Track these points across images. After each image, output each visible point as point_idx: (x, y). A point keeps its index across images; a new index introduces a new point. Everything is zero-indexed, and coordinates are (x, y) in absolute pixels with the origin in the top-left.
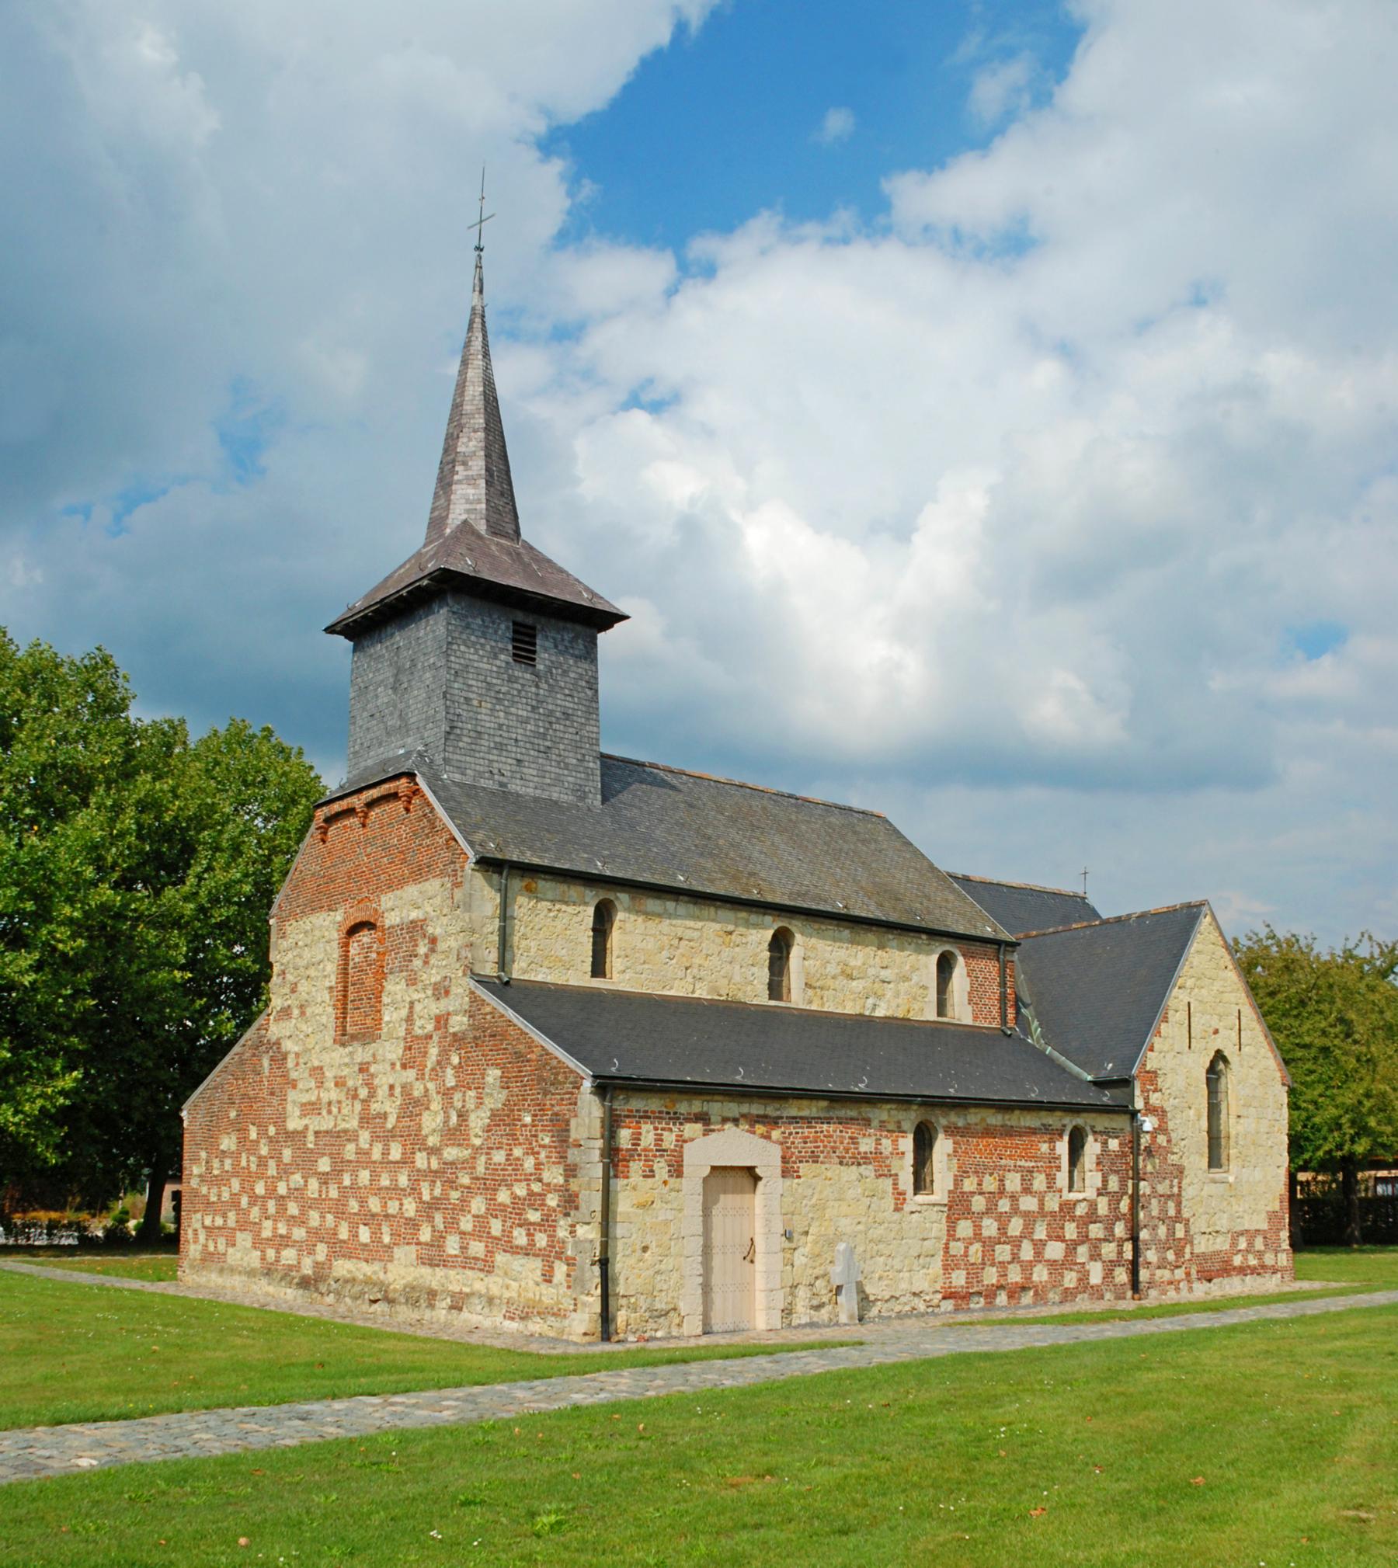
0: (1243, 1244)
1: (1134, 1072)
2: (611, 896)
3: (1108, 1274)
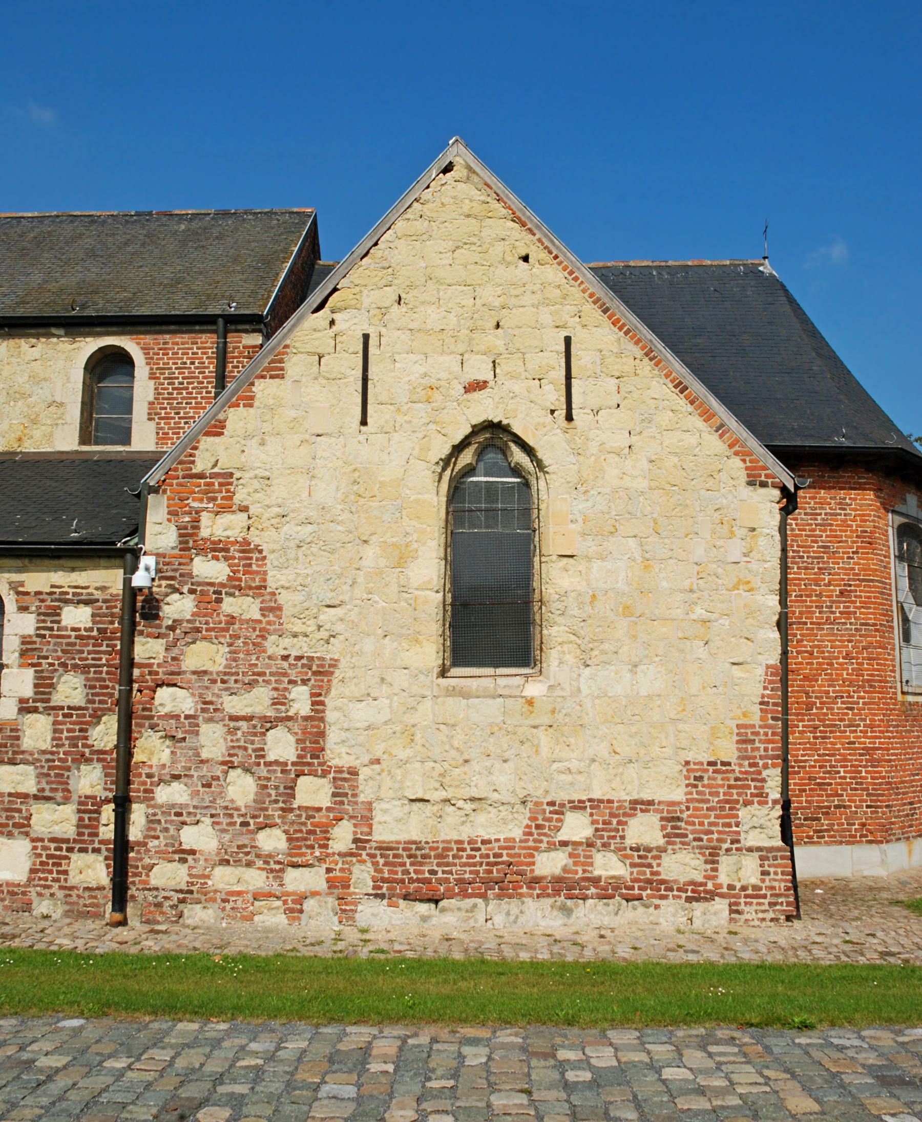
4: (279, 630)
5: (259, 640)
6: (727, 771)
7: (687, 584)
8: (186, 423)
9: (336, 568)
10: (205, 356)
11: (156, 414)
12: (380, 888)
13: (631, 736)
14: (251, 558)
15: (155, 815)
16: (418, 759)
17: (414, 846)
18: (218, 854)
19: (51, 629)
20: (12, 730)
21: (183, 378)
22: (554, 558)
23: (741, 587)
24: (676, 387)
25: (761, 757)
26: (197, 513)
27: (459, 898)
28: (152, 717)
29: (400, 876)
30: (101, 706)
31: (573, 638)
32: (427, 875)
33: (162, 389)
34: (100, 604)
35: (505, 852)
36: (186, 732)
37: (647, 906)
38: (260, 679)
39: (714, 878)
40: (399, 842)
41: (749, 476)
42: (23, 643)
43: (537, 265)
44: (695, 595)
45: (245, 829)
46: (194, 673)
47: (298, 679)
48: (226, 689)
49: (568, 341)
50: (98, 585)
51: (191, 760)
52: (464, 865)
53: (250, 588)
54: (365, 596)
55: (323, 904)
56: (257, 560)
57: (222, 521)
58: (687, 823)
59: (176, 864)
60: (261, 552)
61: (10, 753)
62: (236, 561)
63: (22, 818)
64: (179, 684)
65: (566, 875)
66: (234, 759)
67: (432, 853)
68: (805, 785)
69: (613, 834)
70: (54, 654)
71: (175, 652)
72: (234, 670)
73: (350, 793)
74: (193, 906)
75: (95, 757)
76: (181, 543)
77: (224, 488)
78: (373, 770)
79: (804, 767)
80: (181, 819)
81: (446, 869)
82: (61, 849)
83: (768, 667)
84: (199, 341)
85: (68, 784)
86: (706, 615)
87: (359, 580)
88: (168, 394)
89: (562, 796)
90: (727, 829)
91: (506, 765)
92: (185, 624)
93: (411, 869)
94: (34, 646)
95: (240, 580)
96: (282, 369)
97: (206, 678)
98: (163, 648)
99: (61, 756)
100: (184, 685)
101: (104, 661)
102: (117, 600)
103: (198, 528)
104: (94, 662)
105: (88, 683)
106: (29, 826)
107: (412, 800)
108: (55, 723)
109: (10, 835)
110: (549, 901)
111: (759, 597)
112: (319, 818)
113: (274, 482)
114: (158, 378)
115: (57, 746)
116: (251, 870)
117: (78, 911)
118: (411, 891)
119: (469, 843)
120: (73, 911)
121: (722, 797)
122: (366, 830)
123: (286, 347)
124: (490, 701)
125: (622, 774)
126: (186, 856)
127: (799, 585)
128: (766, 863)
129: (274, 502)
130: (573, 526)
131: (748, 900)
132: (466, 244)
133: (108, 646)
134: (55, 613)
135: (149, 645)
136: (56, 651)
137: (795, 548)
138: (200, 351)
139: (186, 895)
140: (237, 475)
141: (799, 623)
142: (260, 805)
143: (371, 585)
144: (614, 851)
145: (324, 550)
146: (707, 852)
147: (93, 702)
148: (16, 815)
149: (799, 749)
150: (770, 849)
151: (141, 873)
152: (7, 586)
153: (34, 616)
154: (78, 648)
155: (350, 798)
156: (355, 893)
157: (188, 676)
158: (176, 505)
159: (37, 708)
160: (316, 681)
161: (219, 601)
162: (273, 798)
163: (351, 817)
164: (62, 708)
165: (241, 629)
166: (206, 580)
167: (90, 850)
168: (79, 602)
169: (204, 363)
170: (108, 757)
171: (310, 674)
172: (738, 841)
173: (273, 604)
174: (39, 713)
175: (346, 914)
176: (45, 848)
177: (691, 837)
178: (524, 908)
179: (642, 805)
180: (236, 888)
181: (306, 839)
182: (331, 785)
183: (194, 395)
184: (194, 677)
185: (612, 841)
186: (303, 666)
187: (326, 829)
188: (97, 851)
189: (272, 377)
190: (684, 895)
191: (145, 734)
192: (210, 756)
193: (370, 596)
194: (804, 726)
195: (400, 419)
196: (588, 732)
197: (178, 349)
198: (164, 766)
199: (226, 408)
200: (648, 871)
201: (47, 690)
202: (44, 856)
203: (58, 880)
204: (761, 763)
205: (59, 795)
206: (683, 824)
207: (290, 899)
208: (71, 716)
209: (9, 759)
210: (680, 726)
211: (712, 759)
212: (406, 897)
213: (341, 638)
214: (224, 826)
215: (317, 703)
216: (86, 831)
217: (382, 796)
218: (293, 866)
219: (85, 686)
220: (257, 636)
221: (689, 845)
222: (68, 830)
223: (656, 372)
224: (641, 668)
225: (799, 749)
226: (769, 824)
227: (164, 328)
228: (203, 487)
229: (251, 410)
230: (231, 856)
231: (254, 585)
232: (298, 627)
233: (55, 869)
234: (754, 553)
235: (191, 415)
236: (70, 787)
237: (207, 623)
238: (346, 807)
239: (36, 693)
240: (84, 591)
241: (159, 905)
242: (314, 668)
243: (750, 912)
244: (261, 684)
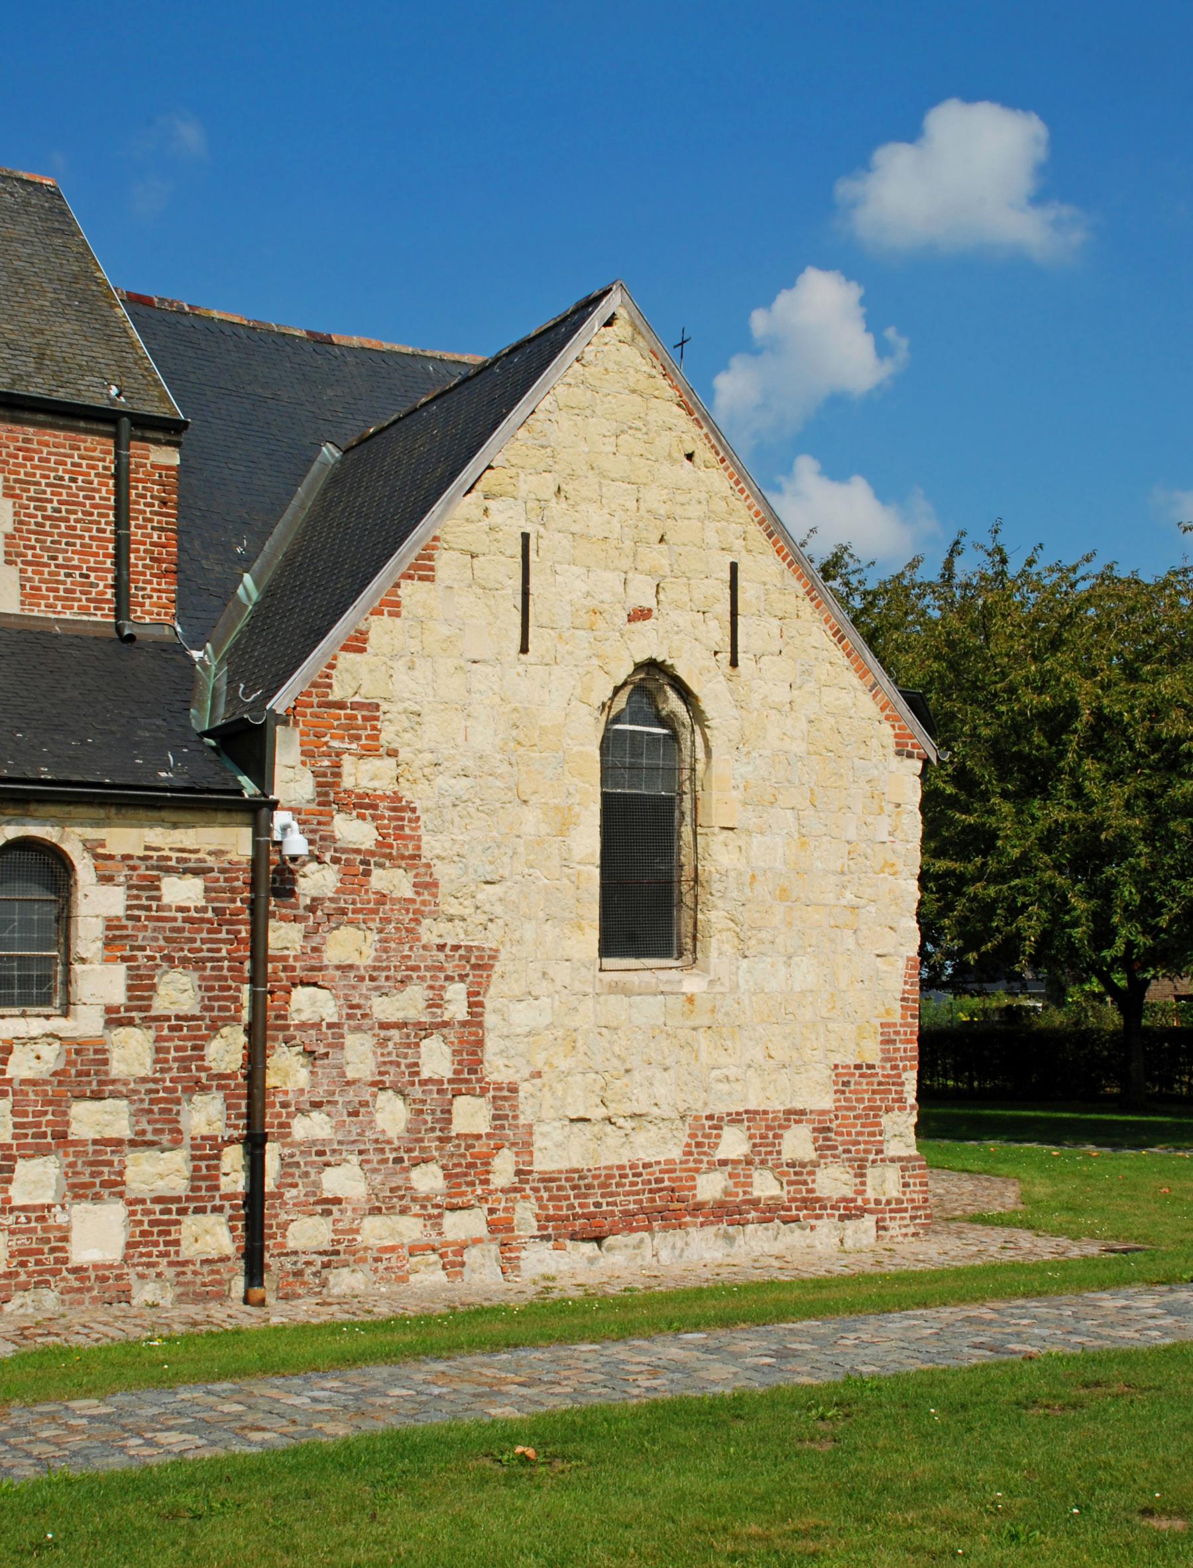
0: (733, 1144)
1: (280, 702)
4: (435, 912)
5: (413, 925)
6: (872, 1075)
7: (838, 866)
8: (68, 575)
9: (495, 834)
10: (93, 472)
11: (19, 555)
12: (546, 1228)
13: (785, 1038)
14: (402, 819)
15: (292, 1156)
16: (580, 1070)
17: (576, 1176)
18: (369, 1200)
19: (149, 908)
20: (96, 1052)
21: (60, 502)
22: (716, 830)
23: (887, 870)
24: (834, 635)
25: (902, 1059)
26: (338, 755)
27: (625, 1233)
28: (287, 1027)
29: (564, 1212)
30: (222, 1014)
31: (732, 925)
32: (592, 1209)
33: (26, 515)
34: (215, 874)
35: (666, 1176)
36: (329, 1045)
37: (803, 1228)
38: (415, 975)
39: (862, 1192)
40: (560, 1172)
41: (898, 744)
42: (108, 928)
43: (703, 468)
44: (845, 878)
45: (399, 1166)
46: (338, 968)
47: (455, 975)
48: (377, 988)
49: (734, 567)
50: (212, 848)
51: (334, 1082)
53: (403, 857)
54: (526, 871)
55: (486, 1253)
56: (410, 821)
57: (368, 767)
58: (837, 1133)
59: (317, 1217)
60: (414, 810)
61: (95, 1083)
62: (386, 822)
63: (115, 1173)
64: (320, 983)
65: (728, 1199)
66: (386, 1078)
67: (596, 1183)
69: (769, 1149)
70: (155, 944)
71: (316, 941)
72: (384, 964)
73: (511, 1114)
74: (341, 1270)
75: (214, 1083)
76: (319, 794)
77: (368, 724)
78: (533, 1085)
80: (323, 1158)
81: (610, 1200)
82: (169, 1211)
83: (909, 959)
84: (82, 445)
85: (178, 1122)
86: (856, 901)
87: (518, 850)
88: (37, 524)
89: (720, 1109)
90: (872, 1139)
91: (666, 1075)
92: (327, 904)
94: (125, 933)
95: (391, 846)
96: (432, 569)
97: (352, 975)
98: (301, 936)
99: (168, 1084)
100: (326, 984)
101: (224, 953)
102: (238, 870)
103: (339, 775)
104: (210, 955)
105: (204, 984)
106: (123, 1183)
107: (572, 1120)
108: (158, 1039)
109: (97, 1198)
110: (712, 1230)
111: (902, 882)
112: (480, 1147)
113: (425, 719)
114: (19, 497)
115: (162, 1070)
116: (405, 1218)
117: (195, 1293)
118: (577, 1229)
119: (631, 1168)
120: (187, 1294)
121: (867, 1104)
122: (527, 1158)
123: (436, 539)
124: (651, 999)
125: (775, 1081)
126: (330, 1207)
129: (426, 747)
130: (734, 793)
132: (631, 428)
133: (228, 932)
134: (153, 886)
135: (282, 931)
136: (156, 939)
138: (84, 462)
139: (331, 1257)
140: (384, 707)
142: (414, 1132)
143: (532, 857)
144: (771, 1169)
145: (482, 811)
146: (856, 1164)
147: (211, 1009)
148: (106, 1169)
150: (909, 1159)
151: (276, 1233)
152: (80, 845)
153: (122, 889)
154: (186, 934)
155: (511, 1121)
156: (519, 1237)
157: (331, 972)
158: (311, 743)
159: (132, 1018)
160: (474, 976)
161: (367, 873)
162: (430, 1125)
163: (513, 1144)
164: (168, 1018)
165: (392, 910)
166: (351, 846)
167: (209, 1209)
168: (186, 871)
169: (91, 483)
170: (232, 1083)
171: (468, 967)
172: (879, 1152)
173: (428, 879)
174: (134, 1026)
175: (509, 1264)
176: (147, 1212)
177: (841, 1148)
178: (689, 1239)
179: (795, 1115)
180: (388, 1243)
181: (466, 1174)
182: (490, 1106)
183: (78, 532)
184: (338, 973)
185: (769, 1157)
186: (461, 957)
187: (486, 1160)
188: (218, 1209)
189: (421, 578)
190: (837, 1213)
191: (279, 1050)
192: (357, 1076)
193: (531, 871)
196: (746, 1034)
197: (49, 453)
198: (302, 1091)
199: (367, 615)
200: (804, 1188)
201: (146, 994)
202: (146, 1223)
203: (167, 1254)
204: (901, 1065)
205: (166, 1138)
206: (832, 1135)
207: (450, 1250)
208: (180, 1028)
209: (92, 1092)
210: (831, 1026)
212: (573, 1237)
213: (500, 922)
214: (375, 1165)
215: (475, 1004)
216: (204, 1184)
217: (543, 1117)
219: (200, 987)
220: (411, 920)
221: (839, 1157)
222: (179, 1185)
223: (816, 615)
224: (796, 959)
227: (27, 416)
228: (343, 721)
229: (397, 620)
230: (384, 1202)
231: (407, 854)
232: (453, 909)
233: (161, 1239)
235: (76, 563)
236: (180, 1127)
237: (354, 903)
239: (130, 999)
240: (192, 856)
241: (298, 1274)
242: (473, 961)
244: (416, 981)
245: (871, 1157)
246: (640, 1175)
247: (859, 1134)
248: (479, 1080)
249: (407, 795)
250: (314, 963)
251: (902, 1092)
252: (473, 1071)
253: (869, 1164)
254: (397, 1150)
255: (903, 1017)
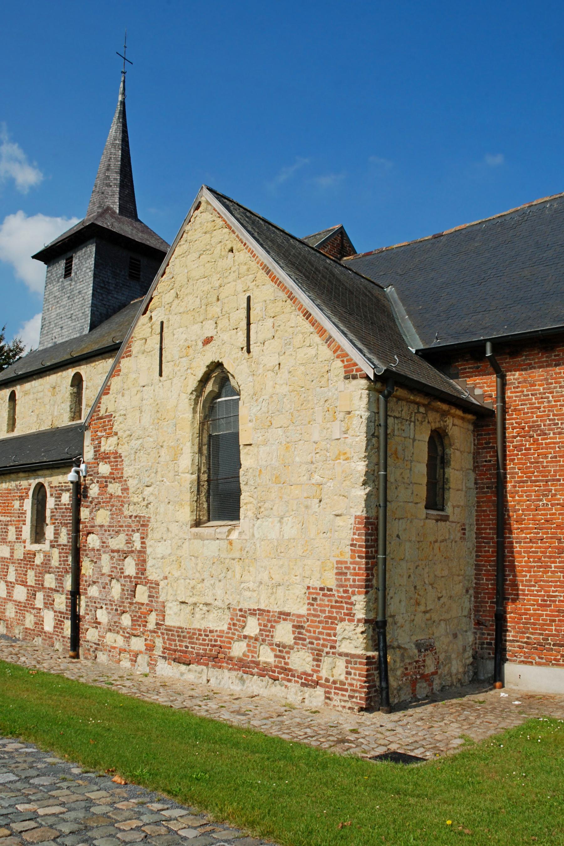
2: (14, 389)
3: (59, 624)
6: (330, 595)
7: (309, 458)
23: (341, 457)
25: (351, 586)
26: (100, 438)
32: (184, 648)
35: (219, 639)
38: (121, 529)
39: (318, 671)
40: (174, 627)
46: (100, 526)
48: (110, 535)
49: (249, 299)
52: (201, 644)
58: (307, 631)
66: (113, 574)
68: (554, 616)
69: (268, 633)
79: (555, 601)
83: (356, 517)
89: (245, 606)
90: (328, 638)
93: (178, 643)
110: (234, 673)
121: (327, 614)
124: (213, 542)
127: (555, 448)
128: (349, 665)
130: (250, 424)
131: (336, 691)
137: (551, 417)
141: (554, 480)
146: (316, 652)
149: (551, 586)
161: (107, 486)
172: (334, 647)
177: (308, 640)
179: (284, 615)
185: (267, 638)
190: (300, 681)
194: (555, 567)
195: (177, 369)
200: (283, 660)
204: (350, 590)
211: (322, 586)
212: (174, 660)
218: (135, 636)
224: (285, 519)
225: (551, 586)
226: (355, 637)
232: (135, 500)
234: (350, 430)
238: (154, 604)
242: (141, 523)
243: (337, 700)
245: (328, 649)
246: (207, 636)
247: (320, 633)
248: (145, 578)
249: (120, 451)
250: (92, 524)
251: (351, 609)
252: (143, 574)
253: (324, 654)
254: (116, 605)
255: (352, 557)
